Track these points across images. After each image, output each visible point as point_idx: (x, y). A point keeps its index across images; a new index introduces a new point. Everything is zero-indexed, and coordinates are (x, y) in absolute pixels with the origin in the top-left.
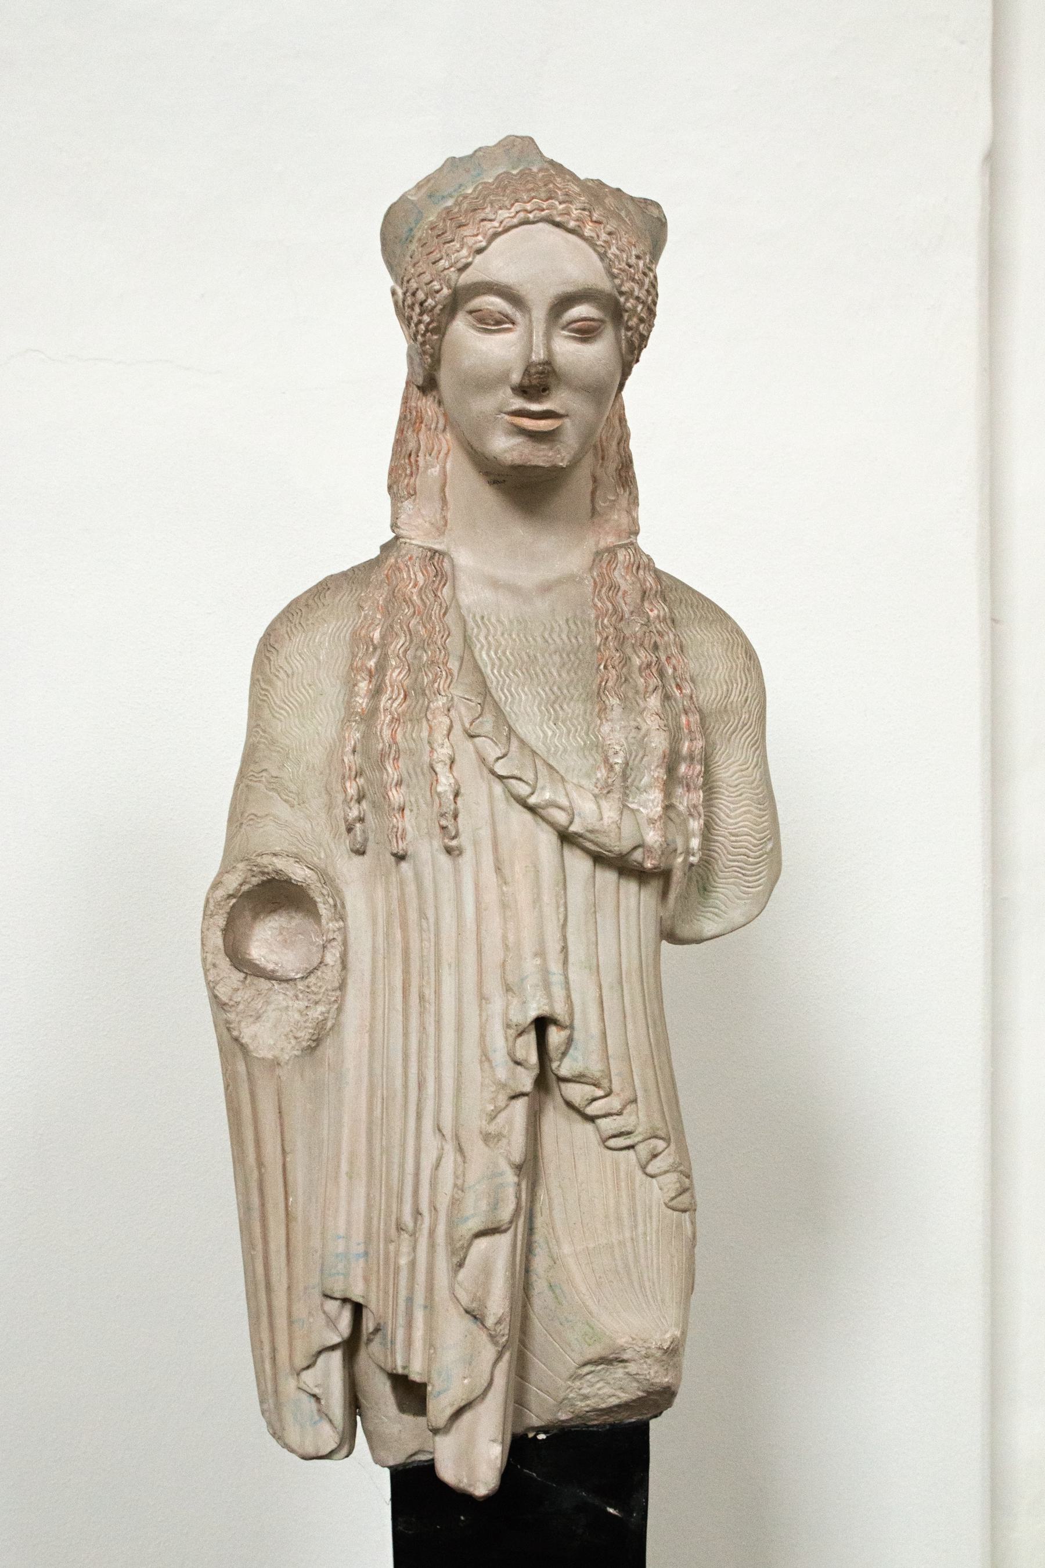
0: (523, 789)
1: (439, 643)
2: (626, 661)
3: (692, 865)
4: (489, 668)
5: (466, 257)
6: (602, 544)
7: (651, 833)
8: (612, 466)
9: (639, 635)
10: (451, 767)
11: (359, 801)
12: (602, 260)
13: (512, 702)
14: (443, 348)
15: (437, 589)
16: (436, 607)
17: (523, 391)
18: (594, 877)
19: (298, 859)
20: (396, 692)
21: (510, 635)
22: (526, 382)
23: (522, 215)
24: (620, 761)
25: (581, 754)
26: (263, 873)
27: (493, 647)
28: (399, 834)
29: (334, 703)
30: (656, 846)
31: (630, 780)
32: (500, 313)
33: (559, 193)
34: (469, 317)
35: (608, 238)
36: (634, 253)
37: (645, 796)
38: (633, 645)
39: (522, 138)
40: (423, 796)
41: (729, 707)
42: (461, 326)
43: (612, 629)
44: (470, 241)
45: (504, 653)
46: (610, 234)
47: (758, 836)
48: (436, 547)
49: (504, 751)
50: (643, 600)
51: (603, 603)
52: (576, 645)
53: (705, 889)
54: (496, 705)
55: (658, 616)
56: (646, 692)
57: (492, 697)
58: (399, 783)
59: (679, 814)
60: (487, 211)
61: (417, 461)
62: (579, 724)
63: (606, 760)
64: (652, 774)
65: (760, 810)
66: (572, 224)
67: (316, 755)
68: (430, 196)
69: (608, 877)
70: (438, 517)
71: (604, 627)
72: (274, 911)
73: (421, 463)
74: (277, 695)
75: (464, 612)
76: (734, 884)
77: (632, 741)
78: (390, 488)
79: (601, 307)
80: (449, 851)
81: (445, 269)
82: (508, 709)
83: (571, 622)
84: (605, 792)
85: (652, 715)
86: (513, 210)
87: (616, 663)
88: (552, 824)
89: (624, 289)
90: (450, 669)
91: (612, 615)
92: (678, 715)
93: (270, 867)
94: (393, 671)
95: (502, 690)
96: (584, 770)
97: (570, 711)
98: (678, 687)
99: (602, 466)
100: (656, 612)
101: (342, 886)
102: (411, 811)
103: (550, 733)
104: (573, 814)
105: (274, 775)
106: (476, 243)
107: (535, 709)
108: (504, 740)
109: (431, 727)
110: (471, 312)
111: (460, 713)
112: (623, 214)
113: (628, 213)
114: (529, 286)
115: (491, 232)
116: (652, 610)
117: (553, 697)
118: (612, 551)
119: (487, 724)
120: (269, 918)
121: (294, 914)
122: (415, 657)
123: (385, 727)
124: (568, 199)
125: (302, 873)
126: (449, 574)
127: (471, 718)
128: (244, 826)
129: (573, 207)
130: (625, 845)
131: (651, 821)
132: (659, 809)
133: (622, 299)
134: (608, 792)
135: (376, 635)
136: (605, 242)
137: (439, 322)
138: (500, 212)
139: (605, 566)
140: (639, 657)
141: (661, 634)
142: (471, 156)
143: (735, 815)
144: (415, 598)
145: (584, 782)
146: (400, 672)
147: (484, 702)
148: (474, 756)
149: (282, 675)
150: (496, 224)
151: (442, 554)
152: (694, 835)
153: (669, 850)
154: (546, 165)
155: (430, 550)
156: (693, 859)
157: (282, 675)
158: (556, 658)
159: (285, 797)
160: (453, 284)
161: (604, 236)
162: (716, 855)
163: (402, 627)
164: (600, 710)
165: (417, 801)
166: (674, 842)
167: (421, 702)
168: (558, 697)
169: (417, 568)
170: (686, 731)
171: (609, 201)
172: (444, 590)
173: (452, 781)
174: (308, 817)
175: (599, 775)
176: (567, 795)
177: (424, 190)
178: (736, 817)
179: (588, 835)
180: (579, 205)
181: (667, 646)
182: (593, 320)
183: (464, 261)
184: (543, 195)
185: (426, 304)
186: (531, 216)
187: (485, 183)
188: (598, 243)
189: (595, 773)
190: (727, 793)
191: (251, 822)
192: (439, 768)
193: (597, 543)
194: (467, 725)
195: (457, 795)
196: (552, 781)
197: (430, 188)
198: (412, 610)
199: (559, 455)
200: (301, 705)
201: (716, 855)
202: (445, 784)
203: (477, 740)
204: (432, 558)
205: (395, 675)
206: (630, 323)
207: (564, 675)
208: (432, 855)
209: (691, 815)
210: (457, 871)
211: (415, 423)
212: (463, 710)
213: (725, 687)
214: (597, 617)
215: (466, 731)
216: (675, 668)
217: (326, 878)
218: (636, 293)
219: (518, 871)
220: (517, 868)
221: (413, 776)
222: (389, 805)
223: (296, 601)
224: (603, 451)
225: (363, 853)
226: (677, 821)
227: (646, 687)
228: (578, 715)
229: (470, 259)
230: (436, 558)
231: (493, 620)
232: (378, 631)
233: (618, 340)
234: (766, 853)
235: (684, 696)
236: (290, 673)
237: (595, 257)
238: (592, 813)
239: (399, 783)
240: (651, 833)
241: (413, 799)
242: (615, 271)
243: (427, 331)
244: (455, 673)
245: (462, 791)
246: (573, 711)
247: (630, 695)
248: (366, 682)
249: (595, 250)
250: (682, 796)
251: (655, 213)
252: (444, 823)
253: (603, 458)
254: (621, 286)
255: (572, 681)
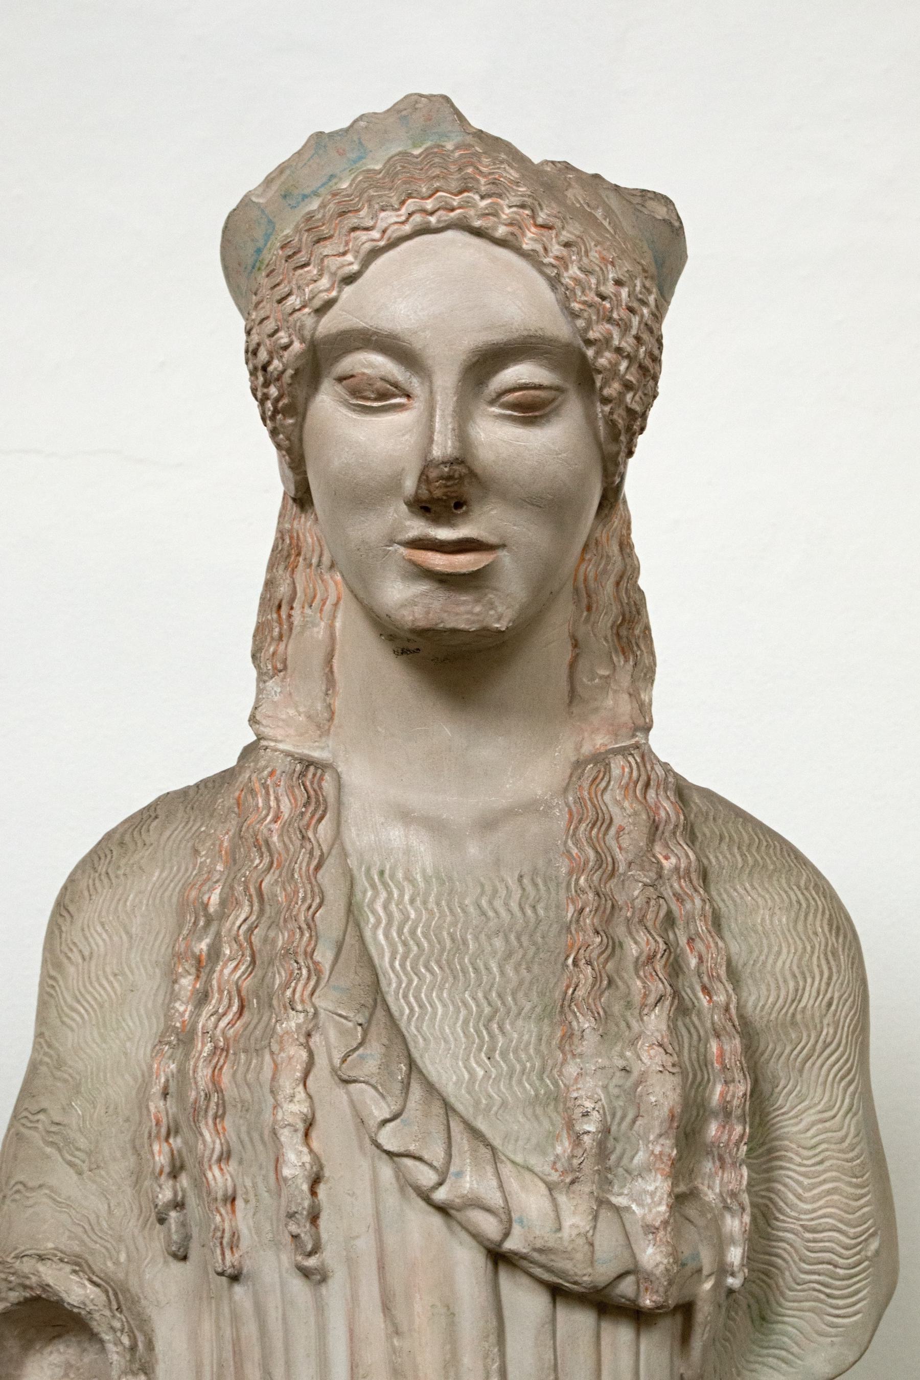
0: (427, 1177)
1: (302, 918)
2: (613, 947)
3: (731, 1291)
4: (387, 959)
5: (327, 290)
6: (587, 749)
7: (650, 1250)
8: (605, 622)
9: (638, 903)
10: (307, 1135)
11: (174, 1175)
12: (554, 288)
13: (421, 1018)
14: (306, 437)
15: (308, 825)
16: (303, 856)
17: (424, 507)
18: (553, 1321)
19: (79, 1264)
20: (225, 1001)
21: (425, 903)
22: (424, 494)
23: (417, 218)
24: (592, 1128)
25: (529, 1112)
26: (25, 1287)
27: (396, 924)
28: (225, 1241)
29: (150, 1005)
30: (658, 1272)
31: (613, 1157)
32: (383, 379)
33: (483, 181)
34: (339, 388)
35: (564, 252)
36: (611, 276)
37: (639, 1184)
38: (628, 920)
39: (430, 97)
40: (265, 1178)
41: (799, 1017)
42: (327, 403)
43: (591, 896)
44: (333, 263)
45: (413, 932)
46: (567, 245)
47: (852, 1231)
48: (316, 754)
49: (395, 1108)
50: (651, 841)
51: (581, 849)
52: (533, 920)
53: (763, 1319)
54: (392, 1021)
55: (677, 869)
56: (644, 1005)
57: (388, 1010)
58: (225, 1156)
59: (705, 1208)
60: (362, 213)
61: (290, 616)
62: (530, 1059)
63: (570, 1125)
64: (651, 1148)
65: (857, 1186)
66: (501, 231)
67: (119, 1090)
68: (285, 197)
69: (577, 1322)
70: (319, 706)
71: (580, 891)
72: (59, 1336)
73: (297, 620)
74: (67, 988)
75: (352, 862)
76: (811, 1310)
77: (616, 1091)
78: (254, 656)
79: (554, 366)
80: (306, 1273)
81: (295, 311)
82: (413, 1029)
83: (526, 881)
84: (568, 1180)
85: (651, 1046)
86: (403, 211)
87: (594, 955)
88: (477, 1236)
89: (592, 335)
90: (316, 963)
91: (595, 870)
92: (703, 1041)
93: (34, 1279)
94: (225, 965)
95: (405, 997)
96: (534, 1141)
97: (515, 1035)
98: (705, 989)
99: (587, 620)
100: (673, 860)
101: (151, 1312)
102: (247, 1201)
103: (480, 1073)
104: (510, 1221)
105: (57, 1119)
106: (343, 266)
107: (459, 1030)
108: (397, 1088)
109: (276, 1065)
110: (340, 379)
111: (327, 1039)
112: (599, 214)
113: (609, 212)
114: (428, 334)
115: (368, 246)
116: (667, 858)
117: (487, 1010)
118: (601, 760)
119: (371, 1060)
120: (49, 1349)
121: (86, 1345)
122: (265, 940)
123: (200, 1064)
124: (497, 190)
125: (81, 1291)
126: (331, 800)
127: (344, 1051)
128: (8, 1202)
129: (503, 203)
130: (603, 1272)
131: (650, 1229)
132: (663, 1208)
133: (590, 353)
134: (573, 1182)
135: (214, 899)
136: (557, 258)
137: (293, 397)
138: (383, 214)
139: (586, 785)
140: (636, 942)
141: (679, 898)
142: (347, 130)
143: (814, 1194)
144: (275, 838)
145: (534, 1161)
146: (236, 967)
147: (369, 1021)
148: (348, 1111)
149: (76, 957)
150: (375, 234)
151: (320, 766)
152: (733, 1242)
153: (684, 1270)
154: (469, 139)
155: (301, 761)
156: (733, 1282)
157: (76, 957)
158: (498, 943)
159: (69, 1158)
160: (307, 334)
161: (556, 249)
162: (780, 1261)
163: (246, 889)
164: (562, 1038)
165: (255, 1185)
166: (696, 1256)
167: (265, 1018)
168: (496, 1011)
169: (281, 790)
170: (717, 1066)
171: (576, 195)
172: (321, 827)
173: (307, 1158)
174: (104, 1193)
175: (559, 1150)
176: (501, 1186)
177: (275, 187)
178: (815, 1199)
179: (536, 1255)
180: (515, 200)
181: (690, 919)
182: (539, 387)
183: (325, 296)
184: (454, 185)
185: (271, 368)
186: (433, 219)
187: (369, 171)
188: (546, 260)
189: (554, 1148)
190: (798, 1159)
191: (17, 1196)
192: (285, 1135)
193: (578, 748)
194: (337, 1062)
195: (316, 1181)
196: (476, 1162)
197: (284, 182)
198: (266, 860)
199: (497, 611)
200: (101, 1006)
201: (780, 1261)
202: (295, 1162)
203: (353, 1087)
204: (303, 774)
205: (227, 972)
206: (606, 392)
207: (510, 971)
208: (281, 1277)
209: (727, 1208)
210: (320, 1309)
211: (289, 556)
212: (332, 1034)
213: (791, 984)
214: (570, 873)
215: (334, 1071)
216: (701, 958)
217: (120, 1296)
218: (616, 342)
219: (421, 1310)
220: (418, 1308)
221: (248, 1145)
222: (209, 1193)
223: (109, 836)
224: (589, 596)
225: (185, 1258)
226: (701, 1222)
227: (646, 996)
228: (528, 1043)
229: (334, 294)
230: (310, 775)
231: (400, 875)
232: (218, 891)
233: (590, 419)
234: (867, 1258)
235: (716, 1006)
236: (87, 954)
237: (542, 285)
238: (544, 1216)
239: (225, 1156)
240: (650, 1250)
241: (249, 1184)
242: (576, 306)
243: (276, 411)
244: (326, 966)
245: (327, 1173)
246: (521, 1035)
247: (616, 1009)
248: (191, 978)
249: (542, 273)
250: (711, 1176)
251: (661, 212)
252: (294, 1228)
253: (589, 608)
254: (586, 330)
255: (521, 983)
